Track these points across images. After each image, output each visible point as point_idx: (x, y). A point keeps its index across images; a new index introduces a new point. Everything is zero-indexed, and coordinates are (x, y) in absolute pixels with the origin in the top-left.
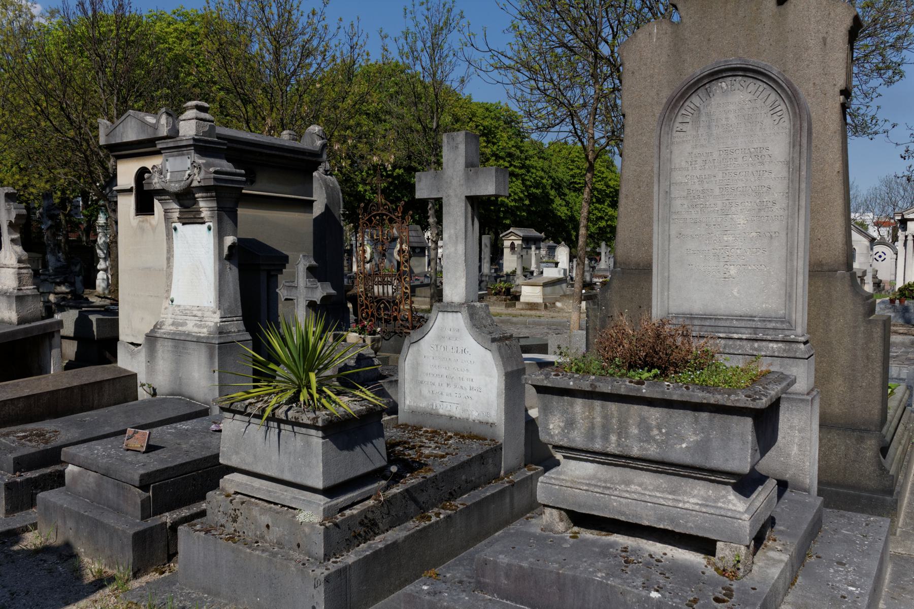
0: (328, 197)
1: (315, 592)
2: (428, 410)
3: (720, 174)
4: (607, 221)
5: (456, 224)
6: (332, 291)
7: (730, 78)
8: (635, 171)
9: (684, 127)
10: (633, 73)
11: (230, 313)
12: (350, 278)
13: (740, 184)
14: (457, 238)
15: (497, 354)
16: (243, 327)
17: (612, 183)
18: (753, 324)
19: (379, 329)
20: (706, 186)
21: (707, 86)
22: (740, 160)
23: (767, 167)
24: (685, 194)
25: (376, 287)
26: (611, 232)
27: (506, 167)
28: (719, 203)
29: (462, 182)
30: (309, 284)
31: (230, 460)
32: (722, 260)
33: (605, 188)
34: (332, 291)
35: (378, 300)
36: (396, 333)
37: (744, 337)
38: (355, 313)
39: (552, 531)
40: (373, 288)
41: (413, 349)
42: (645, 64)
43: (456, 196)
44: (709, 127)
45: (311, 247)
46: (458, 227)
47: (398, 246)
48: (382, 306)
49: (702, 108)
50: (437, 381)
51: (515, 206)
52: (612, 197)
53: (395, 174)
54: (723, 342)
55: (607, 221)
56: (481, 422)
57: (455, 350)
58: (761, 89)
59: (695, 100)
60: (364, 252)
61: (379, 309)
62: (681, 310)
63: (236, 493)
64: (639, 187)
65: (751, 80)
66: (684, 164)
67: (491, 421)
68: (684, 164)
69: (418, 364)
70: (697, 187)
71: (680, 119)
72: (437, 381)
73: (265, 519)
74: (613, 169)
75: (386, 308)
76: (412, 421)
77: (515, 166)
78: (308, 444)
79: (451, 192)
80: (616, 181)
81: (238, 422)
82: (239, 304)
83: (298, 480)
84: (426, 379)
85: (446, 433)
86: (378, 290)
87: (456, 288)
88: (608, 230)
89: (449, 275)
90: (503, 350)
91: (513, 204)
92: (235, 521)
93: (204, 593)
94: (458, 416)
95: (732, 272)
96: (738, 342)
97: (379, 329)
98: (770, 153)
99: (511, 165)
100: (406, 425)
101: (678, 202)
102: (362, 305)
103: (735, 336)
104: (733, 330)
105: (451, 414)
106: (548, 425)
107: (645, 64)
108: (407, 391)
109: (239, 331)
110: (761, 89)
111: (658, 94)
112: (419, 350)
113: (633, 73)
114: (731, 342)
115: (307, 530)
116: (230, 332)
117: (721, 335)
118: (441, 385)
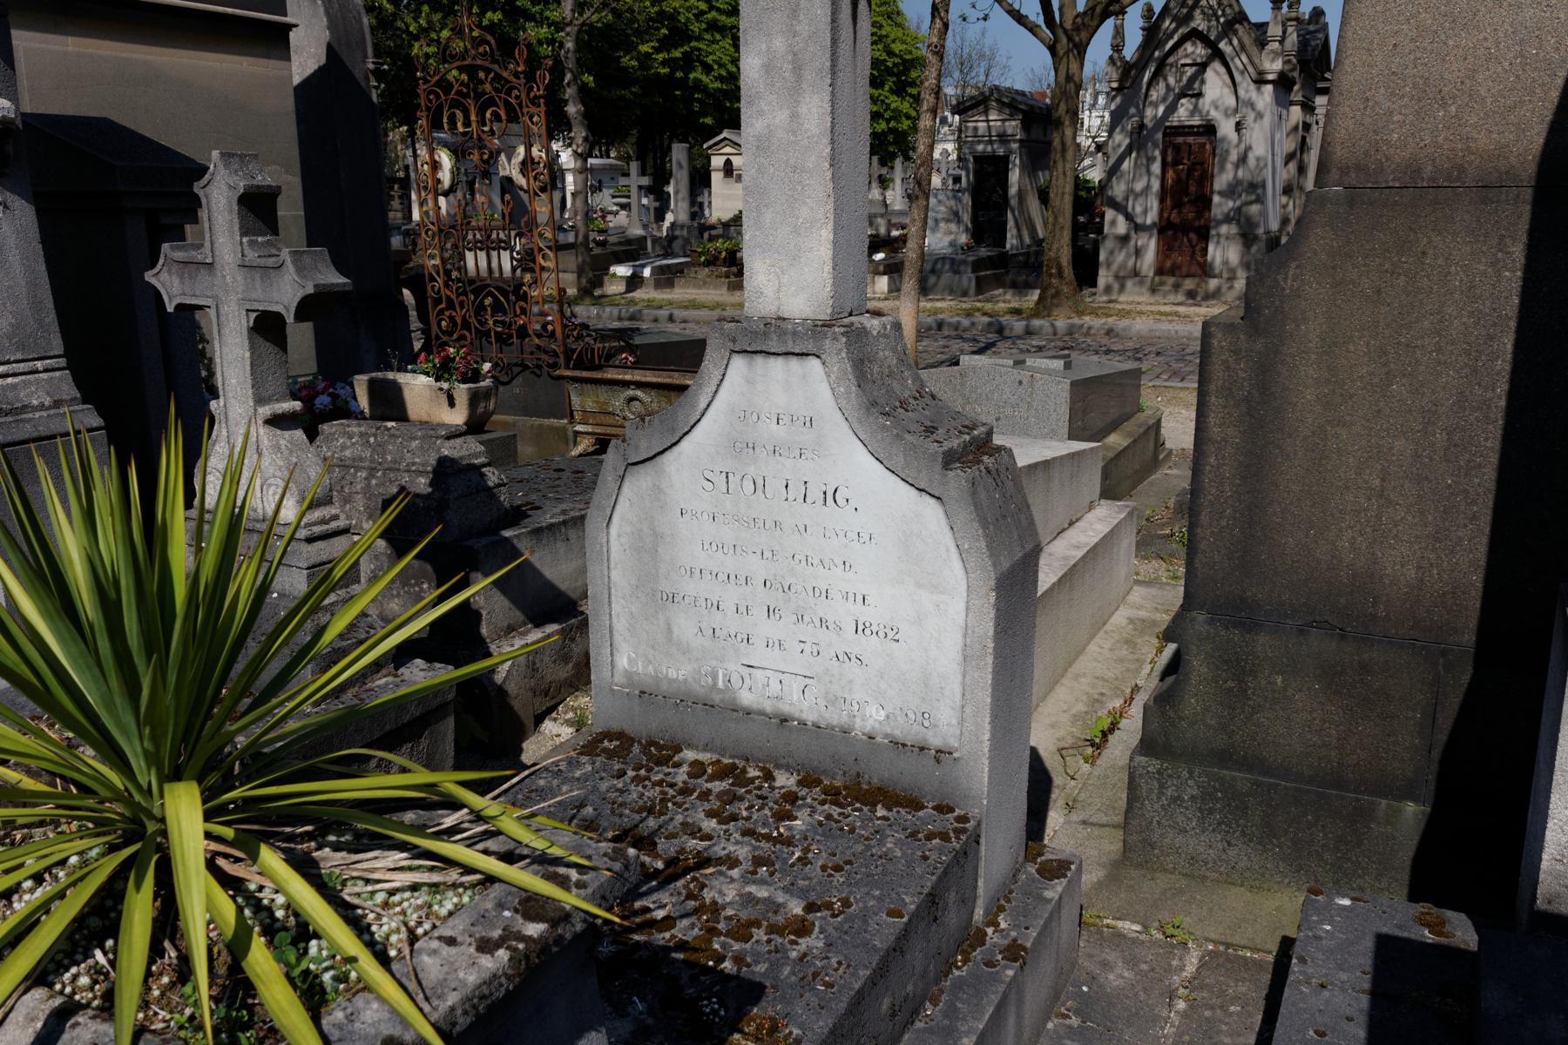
0: (332, 26)
2: (699, 690)
4: (888, 121)
5: (794, 13)
6: (335, 279)
11: (22, 346)
12: (407, 233)
14: (798, 69)
15: (965, 514)
16: (69, 390)
17: (897, 47)
19: (487, 366)
25: (470, 256)
26: (895, 142)
27: (703, 13)
30: (252, 255)
33: (884, 56)
34: (335, 279)
35: (478, 287)
36: (525, 367)
38: (423, 316)
40: (463, 258)
41: (637, 486)
45: (295, 152)
46: (803, 28)
47: (521, 150)
48: (488, 301)
50: (731, 596)
51: (720, 90)
52: (898, 75)
53: (485, 22)
55: (888, 121)
56: (898, 745)
57: (796, 491)
60: (436, 166)
61: (480, 309)
67: (935, 741)
69: (657, 536)
72: (731, 596)
74: (899, 20)
75: (497, 308)
76: (642, 723)
77: (718, 10)
80: (904, 42)
82: (51, 317)
84: (690, 587)
85: (769, 776)
86: (475, 262)
87: (794, 261)
88: (891, 138)
89: (768, 217)
90: (983, 495)
91: (717, 85)
94: (810, 717)
97: (487, 366)
99: (712, 8)
100: (620, 735)
102: (438, 301)
105: (785, 708)
108: (620, 625)
109: (57, 404)
112: (658, 490)
116: (25, 408)
118: (742, 610)
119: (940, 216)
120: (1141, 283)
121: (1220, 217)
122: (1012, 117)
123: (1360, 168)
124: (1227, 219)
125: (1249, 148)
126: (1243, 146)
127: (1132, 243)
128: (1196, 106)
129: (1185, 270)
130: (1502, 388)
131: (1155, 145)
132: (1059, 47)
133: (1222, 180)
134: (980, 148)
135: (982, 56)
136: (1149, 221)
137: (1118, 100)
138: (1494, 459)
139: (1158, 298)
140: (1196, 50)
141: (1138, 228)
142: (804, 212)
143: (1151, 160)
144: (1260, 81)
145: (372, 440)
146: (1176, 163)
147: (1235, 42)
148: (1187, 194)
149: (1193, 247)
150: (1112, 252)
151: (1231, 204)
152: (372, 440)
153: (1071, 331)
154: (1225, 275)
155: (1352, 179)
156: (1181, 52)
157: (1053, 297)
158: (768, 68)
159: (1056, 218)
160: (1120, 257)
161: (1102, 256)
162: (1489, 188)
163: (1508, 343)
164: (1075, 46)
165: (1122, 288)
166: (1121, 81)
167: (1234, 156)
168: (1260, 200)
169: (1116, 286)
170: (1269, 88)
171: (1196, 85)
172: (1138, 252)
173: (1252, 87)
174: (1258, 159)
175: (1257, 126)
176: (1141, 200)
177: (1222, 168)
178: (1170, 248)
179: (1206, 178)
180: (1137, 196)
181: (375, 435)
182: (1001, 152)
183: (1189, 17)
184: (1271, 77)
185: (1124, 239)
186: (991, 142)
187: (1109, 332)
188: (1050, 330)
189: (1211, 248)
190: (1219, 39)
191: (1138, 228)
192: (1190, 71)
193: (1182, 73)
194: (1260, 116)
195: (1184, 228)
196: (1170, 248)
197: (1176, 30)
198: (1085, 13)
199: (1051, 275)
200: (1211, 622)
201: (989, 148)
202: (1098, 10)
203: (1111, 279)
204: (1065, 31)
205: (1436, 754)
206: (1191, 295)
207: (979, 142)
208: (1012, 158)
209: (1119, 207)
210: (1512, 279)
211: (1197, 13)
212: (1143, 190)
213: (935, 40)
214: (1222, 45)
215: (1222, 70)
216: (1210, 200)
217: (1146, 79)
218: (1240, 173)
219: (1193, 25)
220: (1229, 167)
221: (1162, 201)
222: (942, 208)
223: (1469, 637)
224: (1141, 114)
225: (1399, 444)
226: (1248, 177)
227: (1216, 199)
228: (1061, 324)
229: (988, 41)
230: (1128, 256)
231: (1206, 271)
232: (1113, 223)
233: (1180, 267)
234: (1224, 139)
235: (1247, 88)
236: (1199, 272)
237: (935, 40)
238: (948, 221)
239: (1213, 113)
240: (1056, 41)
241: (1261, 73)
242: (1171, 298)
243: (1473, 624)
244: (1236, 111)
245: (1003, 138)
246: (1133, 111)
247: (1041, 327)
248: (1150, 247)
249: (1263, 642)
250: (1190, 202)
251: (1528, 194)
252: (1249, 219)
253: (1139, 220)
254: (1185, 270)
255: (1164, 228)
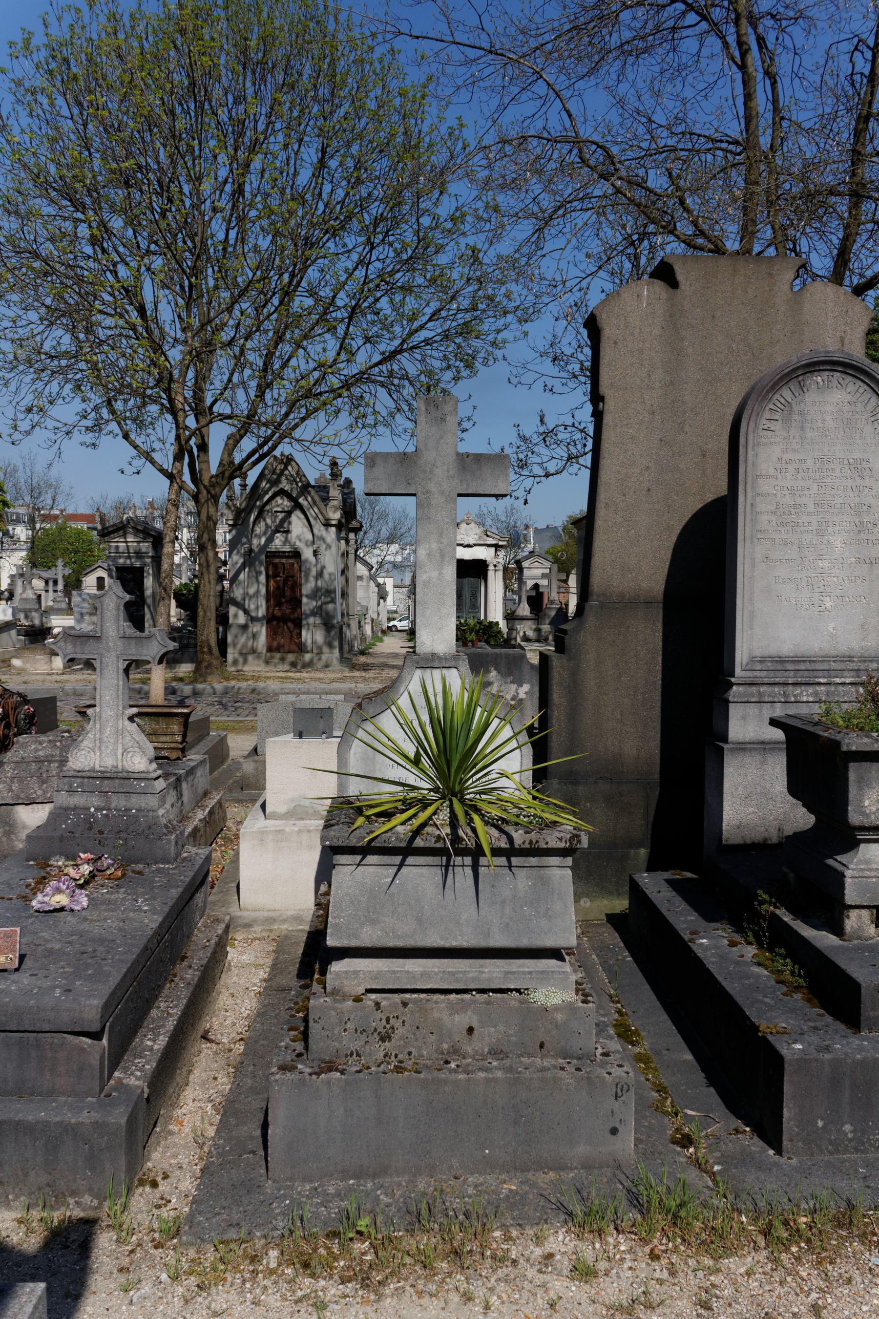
1: (617, 1105)
3: (816, 487)
5: (441, 535)
7: (827, 373)
8: (619, 473)
9: (772, 425)
10: (615, 343)
13: (838, 500)
18: (854, 666)
20: (799, 500)
21: (800, 378)
22: (838, 470)
23: (867, 482)
24: (772, 508)
28: (814, 522)
29: (452, 472)
31: (356, 936)
32: (817, 590)
37: (848, 681)
39: (859, 938)
42: (632, 335)
43: (442, 493)
44: (802, 428)
49: (794, 404)
54: (823, 688)
58: (861, 390)
59: (786, 393)
62: (767, 653)
63: (369, 991)
64: (624, 495)
65: (850, 378)
66: (772, 471)
68: (772, 471)
70: (788, 500)
71: (767, 415)
73: (463, 1020)
78: (544, 882)
79: (432, 487)
81: (371, 869)
83: (524, 942)
89: (428, 612)
92: (385, 1038)
93: (345, 1178)
95: (828, 605)
96: (841, 688)
98: (870, 466)
101: (764, 518)
103: (838, 680)
104: (833, 673)
106: (861, 802)
107: (632, 335)
110: (861, 390)
111: (649, 376)
113: (615, 343)
114: (833, 688)
115: (559, 1017)
117: (822, 680)
119: (84, 611)
120: (259, 657)
121: (308, 612)
122: (144, 540)
123: (604, 595)
124: (313, 614)
125: (323, 568)
126: (319, 566)
127: (250, 630)
128: (286, 538)
129: (286, 648)
130: (659, 676)
131: (261, 564)
132: (201, 496)
133: (307, 588)
134: (121, 561)
135: (50, 486)
136: (260, 615)
137: (234, 532)
138: (659, 704)
139: (271, 667)
140: (283, 503)
141: (253, 619)
142: (444, 611)
143: (259, 573)
144: (327, 525)
145: (58, 744)
146: (275, 575)
147: (309, 499)
148: (284, 597)
149: (291, 632)
150: (236, 636)
151: (314, 603)
152: (58, 744)
153: (226, 692)
154: (315, 651)
155: (602, 599)
156: (273, 503)
157: (207, 667)
158: (429, 555)
159: (205, 612)
160: (242, 640)
161: (230, 639)
162: (648, 603)
163: (660, 659)
164: (212, 496)
165: (245, 661)
166: (235, 519)
167: (314, 572)
168: (333, 601)
169: (241, 660)
170: (333, 529)
171: (286, 525)
172: (255, 636)
173: (323, 528)
174: (330, 574)
175: (328, 553)
176: (253, 600)
177: (307, 580)
178: (275, 633)
179: (296, 586)
180: (251, 597)
181: (61, 741)
182: (138, 564)
183: (277, 481)
184: (334, 522)
185: (245, 627)
186: (129, 557)
187: (253, 691)
188: (211, 691)
189: (304, 633)
190: (299, 496)
191: (253, 619)
192: (281, 516)
193: (276, 517)
194: (329, 547)
195: (283, 620)
196: (275, 633)
197: (270, 489)
198: (217, 476)
199: (203, 653)
200: (559, 784)
201: (128, 562)
202: (227, 474)
203: (237, 655)
204: (205, 486)
205: (650, 827)
206: (293, 665)
207: (120, 557)
208: (146, 569)
209: (239, 605)
210: (659, 635)
211: (283, 478)
212: (253, 592)
213: (173, 497)
214: (301, 500)
215: (302, 516)
216: (300, 601)
217: (252, 519)
218: (319, 583)
219: (281, 486)
220: (312, 579)
221: (268, 601)
222: (86, 605)
223: (657, 776)
224: (250, 542)
225: (626, 700)
226: (324, 585)
227: (304, 600)
228: (218, 687)
229: (54, 473)
230: (248, 639)
231: (301, 648)
232: (236, 616)
233: (283, 646)
234: (306, 561)
235: (319, 529)
236: (296, 649)
237: (173, 497)
238: (91, 614)
239: (298, 544)
240: (199, 492)
241: (327, 520)
242: (280, 667)
243: (658, 769)
244: (313, 542)
245: (139, 554)
246: (244, 540)
247: (204, 689)
248: (263, 632)
249: (581, 789)
250: (286, 602)
251: (661, 605)
252: (327, 613)
253: (253, 614)
254: (286, 648)
255: (270, 620)
